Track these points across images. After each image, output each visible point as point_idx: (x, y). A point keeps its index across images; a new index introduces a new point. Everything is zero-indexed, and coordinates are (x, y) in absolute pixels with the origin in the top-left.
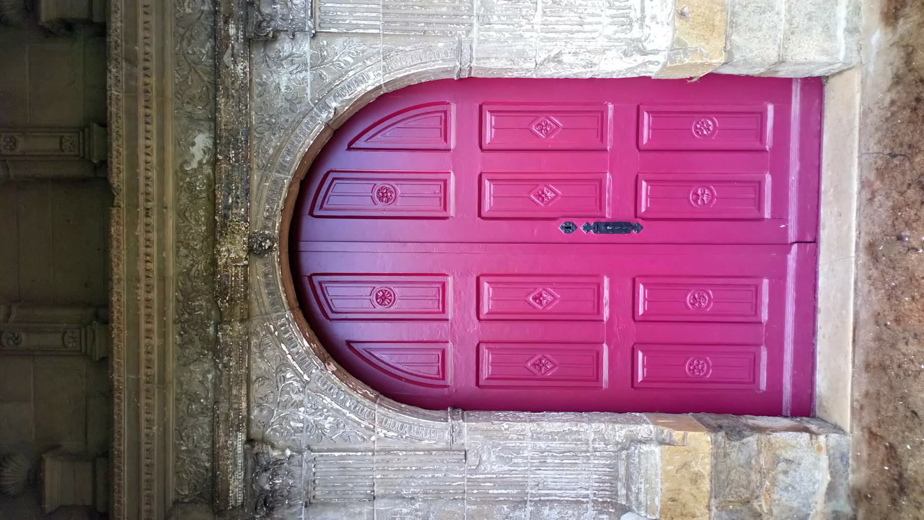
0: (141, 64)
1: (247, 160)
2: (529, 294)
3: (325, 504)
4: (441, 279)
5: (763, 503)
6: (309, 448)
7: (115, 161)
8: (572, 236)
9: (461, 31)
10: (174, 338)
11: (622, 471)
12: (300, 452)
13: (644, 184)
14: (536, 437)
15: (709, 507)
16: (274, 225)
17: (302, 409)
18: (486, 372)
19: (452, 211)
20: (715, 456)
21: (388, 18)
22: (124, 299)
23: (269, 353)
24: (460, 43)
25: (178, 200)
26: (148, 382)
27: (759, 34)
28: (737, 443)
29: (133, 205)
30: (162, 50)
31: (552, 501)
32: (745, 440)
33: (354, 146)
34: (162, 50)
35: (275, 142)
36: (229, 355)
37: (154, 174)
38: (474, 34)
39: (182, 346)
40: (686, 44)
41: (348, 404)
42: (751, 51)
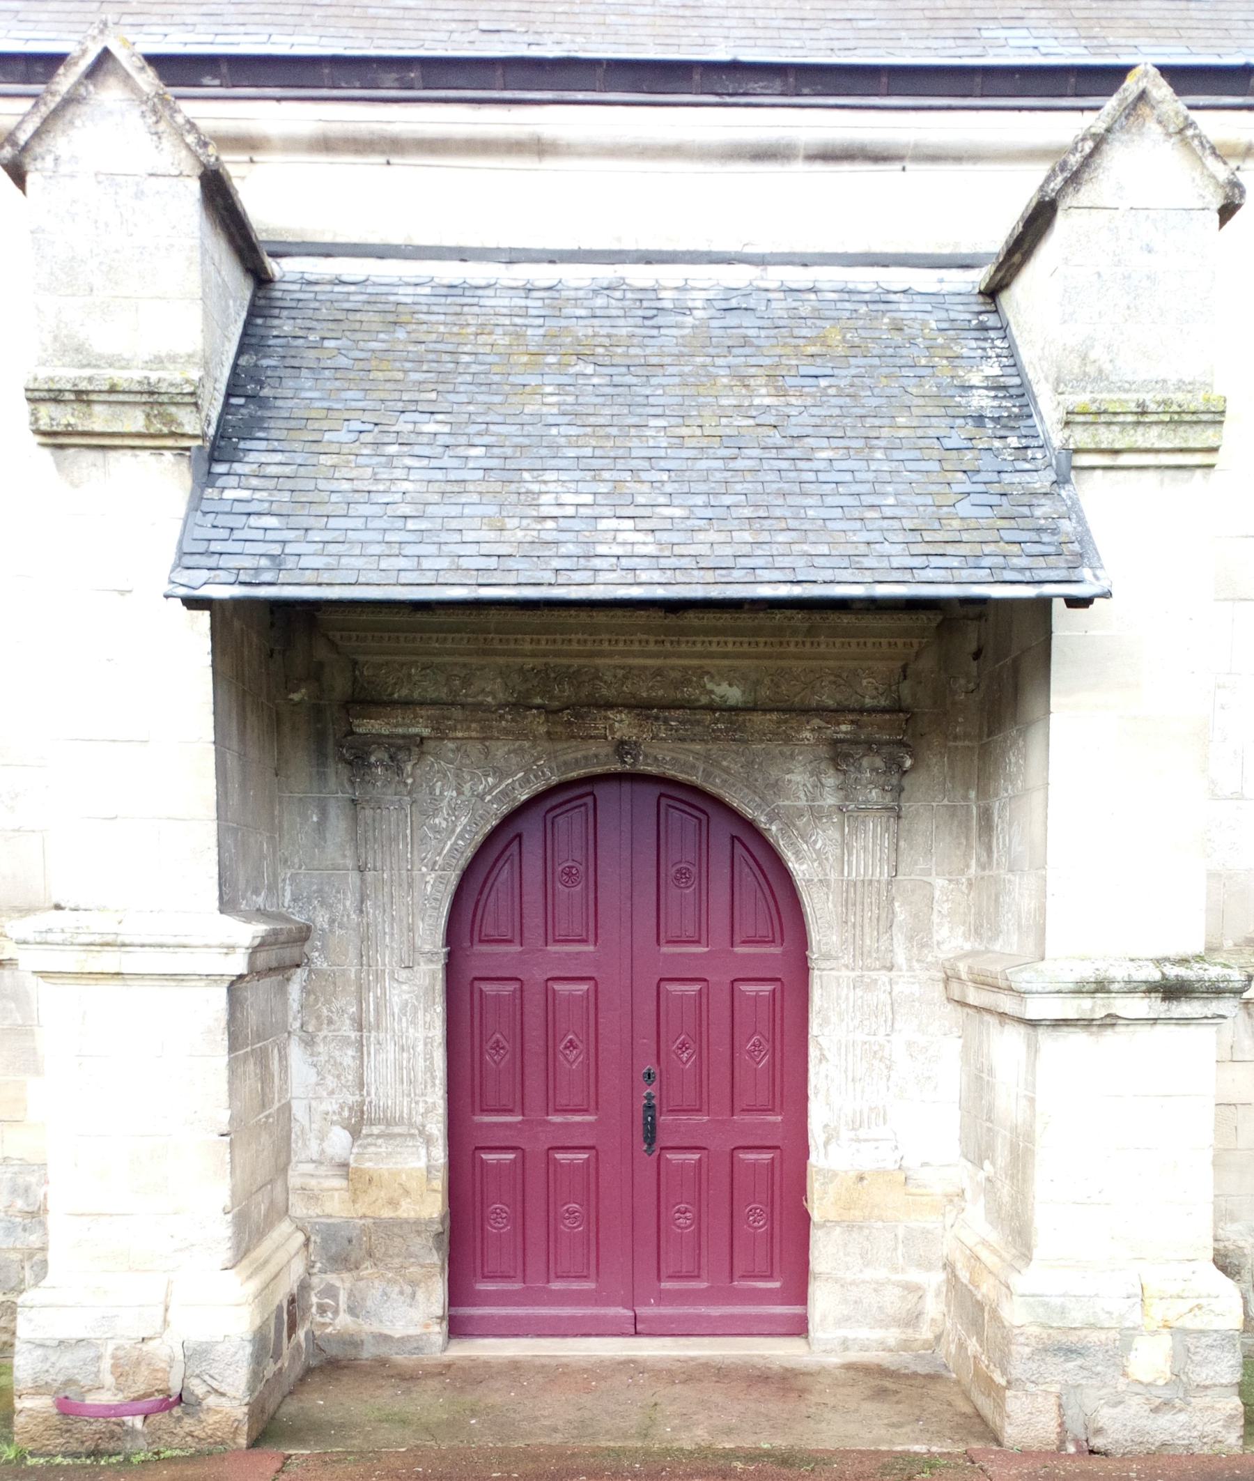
2: (576, 1035)
3: (355, 819)
4: (592, 937)
5: (370, 1271)
7: (711, 615)
8: (639, 1078)
9: (847, 959)
10: (530, 663)
11: (397, 1130)
12: (410, 793)
13: (697, 1156)
14: (428, 1042)
15: (364, 1217)
16: (648, 765)
17: (454, 794)
18: (488, 988)
19: (666, 949)
20: (417, 1222)
21: (859, 885)
22: (572, 621)
23: (514, 759)
24: (837, 958)
25: (673, 668)
26: (485, 639)
27: (841, 1254)
28: (431, 1244)
29: (668, 631)
30: (823, 657)
31: (362, 1058)
32: (434, 1251)
33: (736, 842)
34: (823, 657)
35: (735, 768)
37: (699, 648)
38: (845, 973)
39: (521, 670)
40: (831, 1182)
41: (460, 842)
42: (825, 1247)
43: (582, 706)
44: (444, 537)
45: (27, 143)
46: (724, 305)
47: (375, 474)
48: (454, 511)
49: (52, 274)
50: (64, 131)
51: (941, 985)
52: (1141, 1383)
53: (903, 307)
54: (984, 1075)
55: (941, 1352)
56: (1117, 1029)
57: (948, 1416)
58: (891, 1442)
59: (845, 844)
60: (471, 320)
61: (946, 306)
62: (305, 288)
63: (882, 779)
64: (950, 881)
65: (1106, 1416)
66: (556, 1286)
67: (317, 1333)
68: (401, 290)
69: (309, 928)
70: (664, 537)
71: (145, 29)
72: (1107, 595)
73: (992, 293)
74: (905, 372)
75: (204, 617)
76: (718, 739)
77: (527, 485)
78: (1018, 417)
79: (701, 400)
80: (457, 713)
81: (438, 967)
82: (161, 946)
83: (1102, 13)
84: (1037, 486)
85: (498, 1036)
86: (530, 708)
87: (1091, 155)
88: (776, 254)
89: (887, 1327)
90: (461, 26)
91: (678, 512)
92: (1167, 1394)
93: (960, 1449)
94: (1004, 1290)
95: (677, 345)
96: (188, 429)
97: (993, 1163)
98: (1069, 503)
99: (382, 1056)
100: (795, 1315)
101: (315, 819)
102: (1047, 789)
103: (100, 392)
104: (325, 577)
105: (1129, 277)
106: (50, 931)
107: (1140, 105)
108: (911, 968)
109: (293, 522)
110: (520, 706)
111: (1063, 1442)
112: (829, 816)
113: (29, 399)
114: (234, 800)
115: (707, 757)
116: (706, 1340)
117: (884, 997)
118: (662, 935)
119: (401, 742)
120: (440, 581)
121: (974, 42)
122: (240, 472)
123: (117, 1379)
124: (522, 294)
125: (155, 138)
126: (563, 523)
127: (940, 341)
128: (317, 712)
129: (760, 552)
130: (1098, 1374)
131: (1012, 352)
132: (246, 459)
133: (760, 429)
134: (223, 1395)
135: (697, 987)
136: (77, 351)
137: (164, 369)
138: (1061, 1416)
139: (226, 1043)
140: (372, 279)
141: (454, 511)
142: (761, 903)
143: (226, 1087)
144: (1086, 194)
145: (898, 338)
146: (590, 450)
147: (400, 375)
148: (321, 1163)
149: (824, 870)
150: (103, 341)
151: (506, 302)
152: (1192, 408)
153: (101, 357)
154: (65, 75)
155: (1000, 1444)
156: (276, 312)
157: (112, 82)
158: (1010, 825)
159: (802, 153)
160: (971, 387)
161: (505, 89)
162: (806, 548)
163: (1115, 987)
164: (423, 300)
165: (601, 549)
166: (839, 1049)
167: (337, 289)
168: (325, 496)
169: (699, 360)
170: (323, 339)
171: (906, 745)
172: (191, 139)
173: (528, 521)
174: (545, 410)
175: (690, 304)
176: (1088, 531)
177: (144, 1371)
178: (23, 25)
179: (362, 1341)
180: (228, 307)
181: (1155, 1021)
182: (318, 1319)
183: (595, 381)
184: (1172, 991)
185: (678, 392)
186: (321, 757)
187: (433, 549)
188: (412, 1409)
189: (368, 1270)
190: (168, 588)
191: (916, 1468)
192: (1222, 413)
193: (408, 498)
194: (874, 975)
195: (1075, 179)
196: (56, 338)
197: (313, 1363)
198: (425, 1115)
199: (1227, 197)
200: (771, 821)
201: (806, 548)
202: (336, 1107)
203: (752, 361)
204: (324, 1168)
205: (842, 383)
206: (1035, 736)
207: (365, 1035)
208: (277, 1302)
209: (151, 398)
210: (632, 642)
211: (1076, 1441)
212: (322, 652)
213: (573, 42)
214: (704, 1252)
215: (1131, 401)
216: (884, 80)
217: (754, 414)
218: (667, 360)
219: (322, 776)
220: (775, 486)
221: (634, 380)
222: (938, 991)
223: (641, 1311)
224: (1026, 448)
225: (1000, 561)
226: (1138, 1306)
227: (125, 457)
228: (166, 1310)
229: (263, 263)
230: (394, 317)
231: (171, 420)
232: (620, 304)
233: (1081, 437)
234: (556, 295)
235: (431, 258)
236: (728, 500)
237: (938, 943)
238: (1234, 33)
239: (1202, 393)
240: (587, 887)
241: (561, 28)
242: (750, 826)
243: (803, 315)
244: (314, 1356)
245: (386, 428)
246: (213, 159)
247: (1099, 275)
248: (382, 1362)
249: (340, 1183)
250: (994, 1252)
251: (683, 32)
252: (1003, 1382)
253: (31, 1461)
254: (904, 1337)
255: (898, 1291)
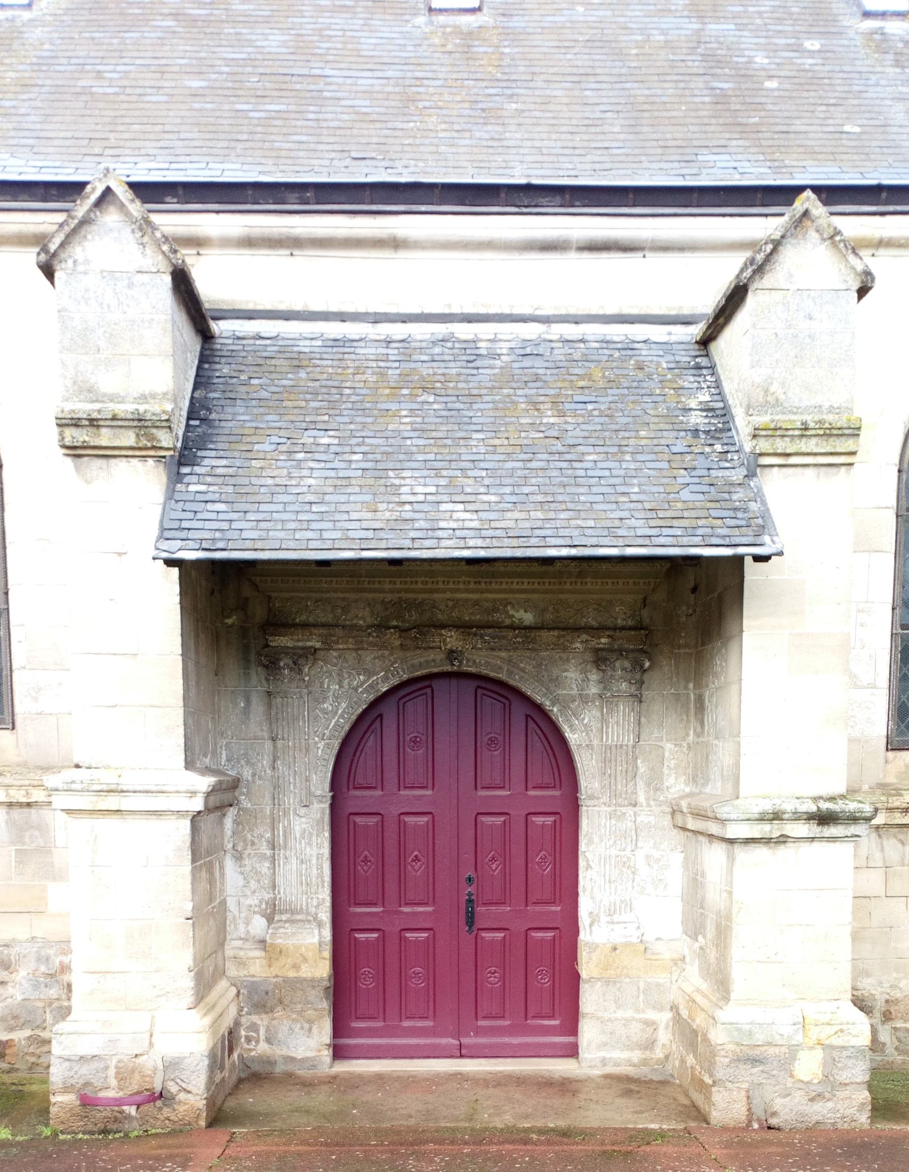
0: (579, 581)
1: (515, 649)
3: (270, 706)
4: (430, 785)
5: (280, 1013)
6: (310, 693)
9: (605, 799)
10: (389, 597)
11: (299, 917)
12: (307, 687)
13: (502, 935)
14: (319, 856)
15: (276, 976)
17: (337, 687)
18: (359, 820)
20: (312, 980)
21: (613, 748)
22: (417, 568)
24: (598, 798)
25: (487, 600)
27: (601, 1000)
28: (322, 995)
30: (590, 592)
31: (274, 868)
34: (590, 592)
35: (529, 668)
36: (377, 636)
37: (504, 586)
42: (590, 995)
43: (425, 627)
44: (337, 516)
45: (55, 251)
46: (522, 352)
47: (290, 473)
48: (343, 498)
49: (72, 339)
50: (80, 243)
51: (669, 816)
52: (802, 1081)
53: (644, 352)
54: (699, 878)
55: (669, 1067)
56: (788, 845)
57: (673, 1106)
58: (635, 1123)
59: (603, 720)
60: (350, 364)
61: (673, 352)
62: (236, 342)
63: (629, 676)
64: (676, 745)
65: (779, 1104)
66: (406, 1024)
67: (245, 1056)
68: (301, 343)
69: (239, 779)
70: (484, 515)
71: (122, 159)
72: (780, 554)
73: (705, 342)
74: (646, 399)
75: (175, 571)
76: (517, 648)
77: (392, 480)
78: (721, 431)
79: (507, 419)
80: (339, 632)
81: (326, 806)
82: (147, 792)
83: (782, 143)
84: (734, 478)
85: (366, 853)
86: (389, 628)
87: (771, 253)
88: (557, 316)
89: (632, 1050)
90: (339, 155)
91: (493, 498)
92: (820, 1089)
93: (681, 1126)
94: (711, 1021)
95: (490, 381)
96: (164, 444)
97: (704, 937)
98: (756, 491)
99: (289, 866)
100: (570, 1043)
101: (242, 705)
102: (740, 683)
103: (106, 419)
104: (259, 545)
105: (797, 336)
106: (73, 782)
107: (804, 219)
108: (649, 805)
109: (237, 507)
110: (382, 626)
111: (750, 1122)
112: (593, 702)
113: (58, 425)
114: (193, 691)
115: (510, 661)
116: (509, 1060)
117: (630, 825)
118: (478, 784)
119: (300, 652)
120: (336, 546)
121: (692, 164)
122: (199, 472)
123: (119, 1082)
124: (384, 345)
125: (141, 247)
126: (416, 507)
127: (669, 377)
128: (243, 631)
129: (548, 526)
130: (774, 1076)
131: (718, 385)
132: (203, 464)
133: (547, 440)
134: (189, 1092)
135: (502, 819)
136: (90, 392)
137: (147, 403)
138: (749, 1104)
139: (190, 857)
140: (281, 335)
141: (343, 498)
142: (546, 762)
143: (189, 886)
144: (768, 280)
145: (640, 375)
146: (433, 455)
147: (303, 404)
148: (247, 940)
149: (589, 738)
150: (108, 383)
151: (373, 351)
152: (839, 425)
153: (105, 395)
154: (81, 205)
155: (708, 1123)
156: (217, 359)
157: (112, 209)
158: (716, 707)
159: (574, 245)
160: (690, 409)
161: (372, 203)
162: (579, 522)
163: (786, 816)
164: (317, 350)
165: (442, 524)
166: (600, 860)
167: (258, 342)
168: (256, 489)
169: (506, 391)
170: (251, 378)
171: (646, 652)
172: (165, 248)
173: (393, 505)
174: (402, 427)
175: (499, 351)
176: (768, 510)
177: (137, 1076)
178: (36, 157)
179: (276, 1062)
180: (187, 358)
181: (813, 839)
182: (246, 1046)
183: (436, 406)
184: (824, 819)
185: (492, 414)
186: (246, 663)
187: (330, 525)
188: (313, 1104)
189: (279, 1013)
190: (154, 553)
191: (652, 1138)
192: (859, 429)
193: (312, 490)
194: (624, 810)
195: (760, 270)
196: (75, 383)
197: (243, 1075)
198: (317, 907)
199: (862, 282)
200: (553, 705)
201: (579, 522)
202: (257, 902)
203: (541, 392)
204: (248, 943)
205: (603, 407)
206: (733, 646)
207: (277, 852)
208: (222, 1033)
209: (140, 423)
210: (459, 582)
211: (759, 1121)
212: (247, 591)
213: (416, 166)
214: (507, 1001)
215: (797, 420)
216: (631, 196)
217: (543, 429)
218: (483, 392)
219: (247, 675)
220: (558, 480)
221: (462, 406)
222: (667, 821)
223: (464, 1041)
224: (727, 452)
225: (709, 530)
226: (801, 1031)
227: (122, 464)
228: (151, 1036)
229: (208, 326)
230: (298, 361)
231: (152, 438)
232: (450, 352)
233: (764, 445)
234: (407, 345)
235: (321, 320)
236: (526, 490)
237: (668, 788)
238: (872, 157)
239: (846, 415)
240: (427, 749)
241: (408, 156)
242: (539, 708)
243: (576, 358)
244: (244, 1071)
245: (295, 441)
246: (180, 261)
247: (776, 334)
248: (290, 1075)
249: (260, 954)
250: (705, 996)
251: (491, 158)
252: (710, 1082)
253: (62, 1137)
254: (644, 1056)
255: (640, 1026)
